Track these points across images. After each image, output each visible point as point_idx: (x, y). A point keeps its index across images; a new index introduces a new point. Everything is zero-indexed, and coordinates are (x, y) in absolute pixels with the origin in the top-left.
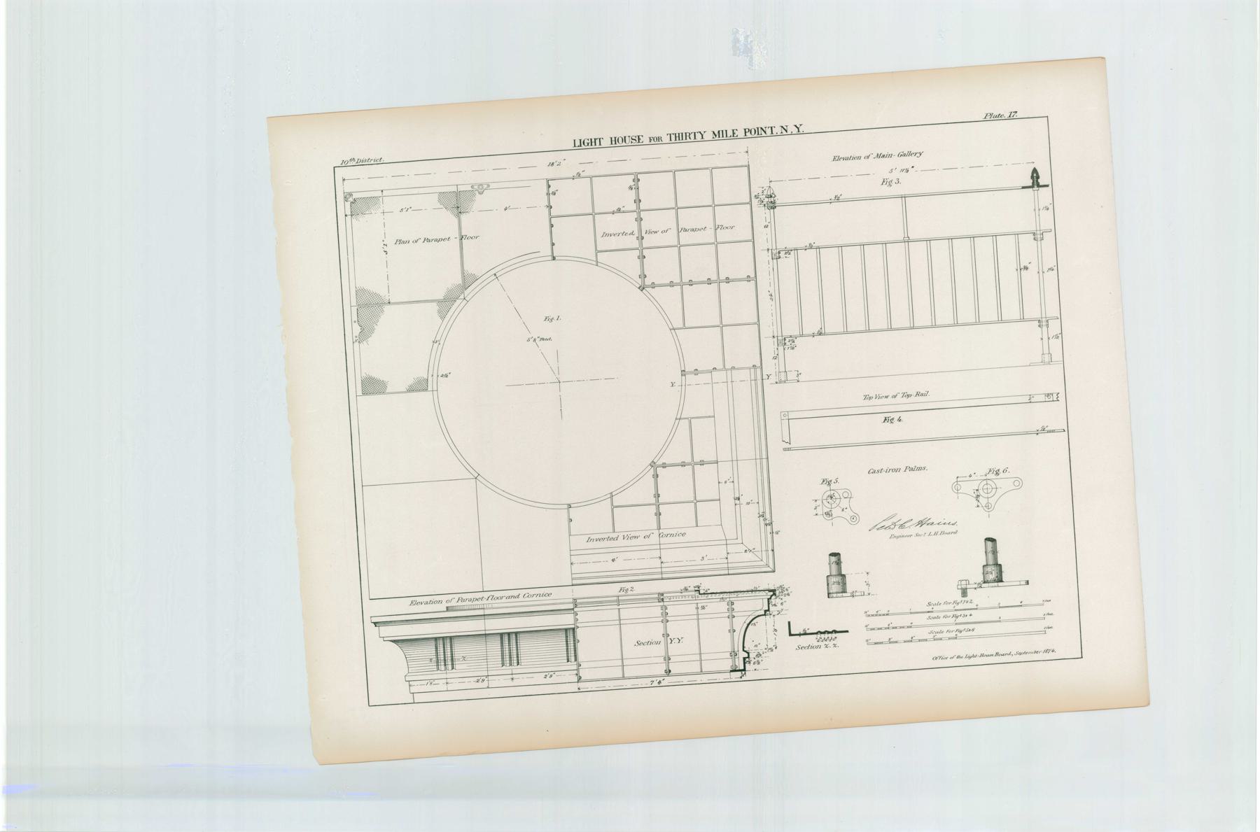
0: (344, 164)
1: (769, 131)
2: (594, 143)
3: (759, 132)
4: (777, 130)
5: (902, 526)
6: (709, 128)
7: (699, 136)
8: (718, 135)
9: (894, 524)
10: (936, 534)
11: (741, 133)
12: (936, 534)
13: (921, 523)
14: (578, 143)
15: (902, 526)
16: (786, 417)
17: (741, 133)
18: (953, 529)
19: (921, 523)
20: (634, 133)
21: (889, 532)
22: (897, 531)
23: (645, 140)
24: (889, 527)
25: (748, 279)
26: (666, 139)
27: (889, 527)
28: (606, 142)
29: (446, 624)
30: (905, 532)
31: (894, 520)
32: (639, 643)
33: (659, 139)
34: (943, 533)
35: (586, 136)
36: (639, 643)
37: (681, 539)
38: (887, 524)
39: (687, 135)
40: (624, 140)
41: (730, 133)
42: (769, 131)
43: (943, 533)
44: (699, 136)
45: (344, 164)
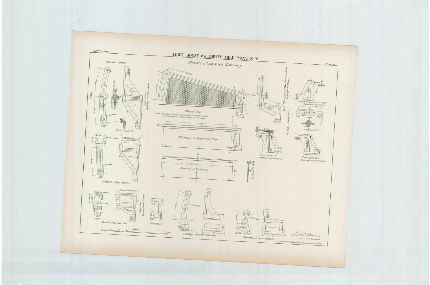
0: (94, 52)
2: (180, 55)
4: (231, 57)
5: (302, 235)
6: (224, 54)
7: (220, 57)
11: (235, 58)
13: (309, 235)
14: (175, 55)
15: (302, 235)
17: (235, 58)
18: (319, 238)
19: (309, 235)
20: (195, 53)
22: (300, 237)
24: (297, 235)
26: (207, 57)
27: (297, 235)
28: (185, 55)
30: (302, 237)
31: (300, 233)
33: (204, 56)
34: (315, 239)
35: (178, 52)
38: (297, 234)
40: (192, 55)
41: (231, 57)
42: (246, 59)
43: (315, 239)
44: (220, 57)
45: (94, 52)
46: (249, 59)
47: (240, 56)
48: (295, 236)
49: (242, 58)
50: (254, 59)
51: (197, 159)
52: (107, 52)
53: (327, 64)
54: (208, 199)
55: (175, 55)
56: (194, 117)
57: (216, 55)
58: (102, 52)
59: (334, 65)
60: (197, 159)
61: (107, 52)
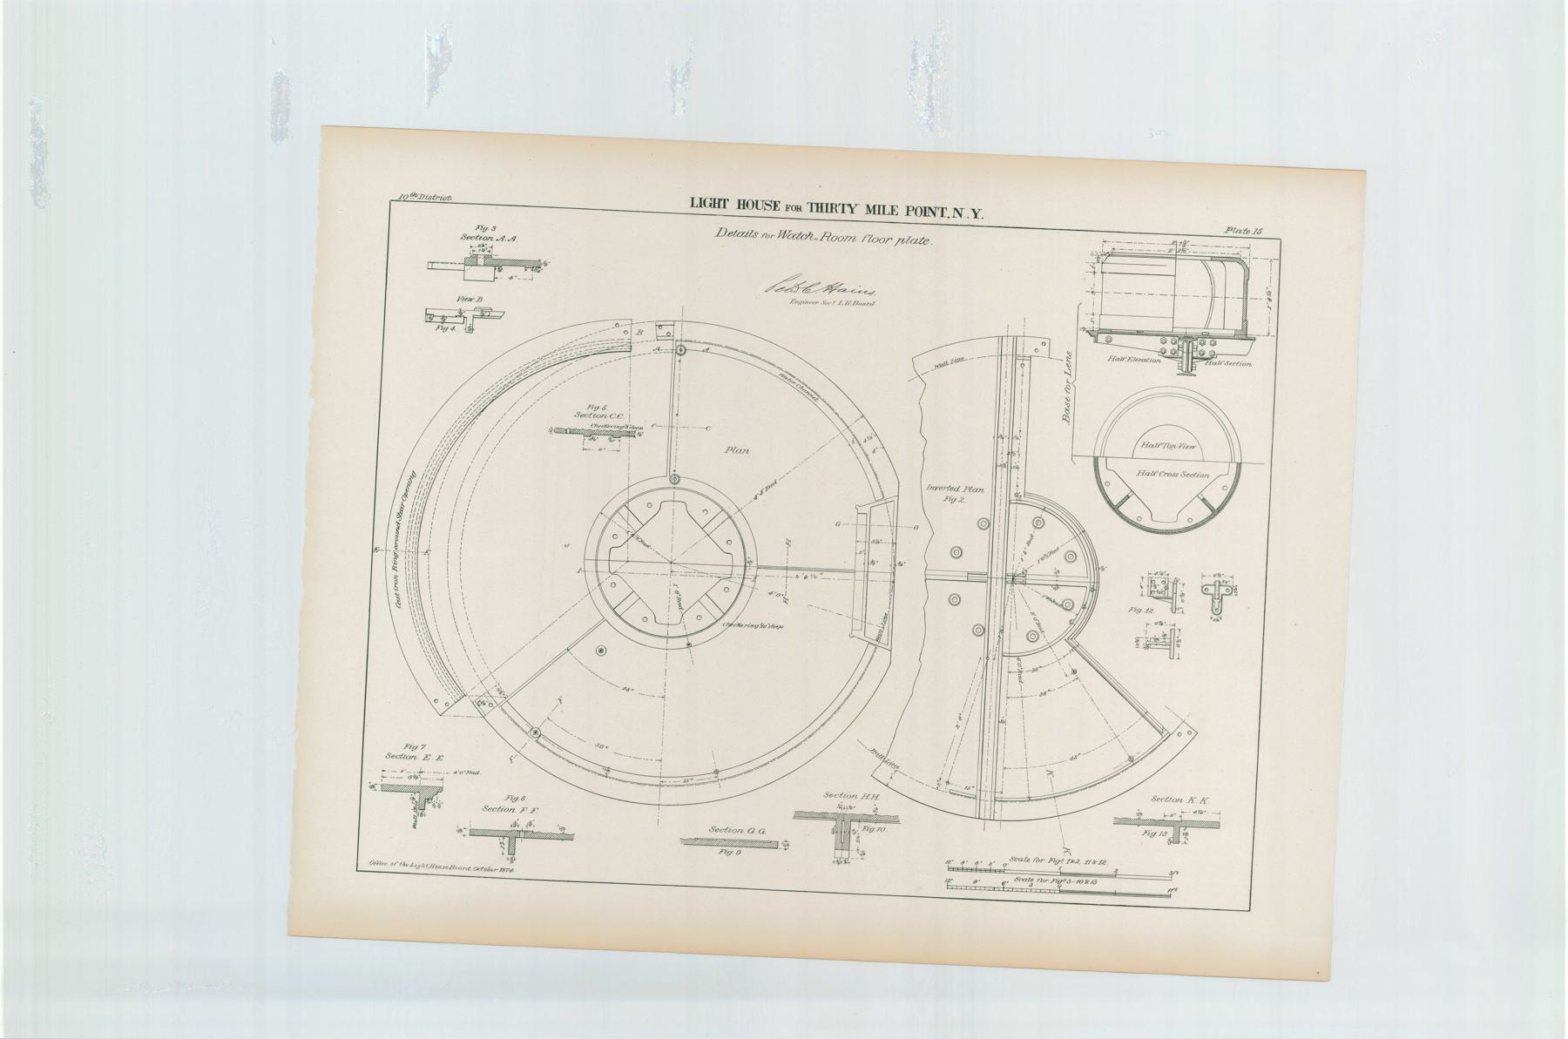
0: (403, 199)
4: (888, 210)
5: (806, 290)
6: (862, 199)
7: (847, 209)
9: (798, 286)
10: (848, 303)
11: (902, 210)
12: (848, 303)
13: (830, 288)
14: (697, 202)
15: (806, 290)
16: (942, 783)
17: (902, 210)
18: (870, 299)
19: (830, 288)
20: (768, 198)
21: (790, 296)
22: (800, 296)
24: (790, 290)
25: (1245, 327)
27: (790, 290)
30: (809, 297)
31: (798, 281)
32: (487, 808)
33: (798, 209)
34: (856, 303)
35: (708, 194)
36: (487, 808)
38: (788, 285)
39: (832, 208)
40: (755, 204)
41: (888, 210)
42: (939, 213)
43: (856, 303)
44: (847, 209)
45: (403, 199)
48: (782, 293)
49: (924, 211)
51: (717, 772)
52: (446, 200)
55: (697, 202)
56: (957, 741)
57: (717, 196)
58: (432, 199)
60: (717, 772)
61: (446, 200)
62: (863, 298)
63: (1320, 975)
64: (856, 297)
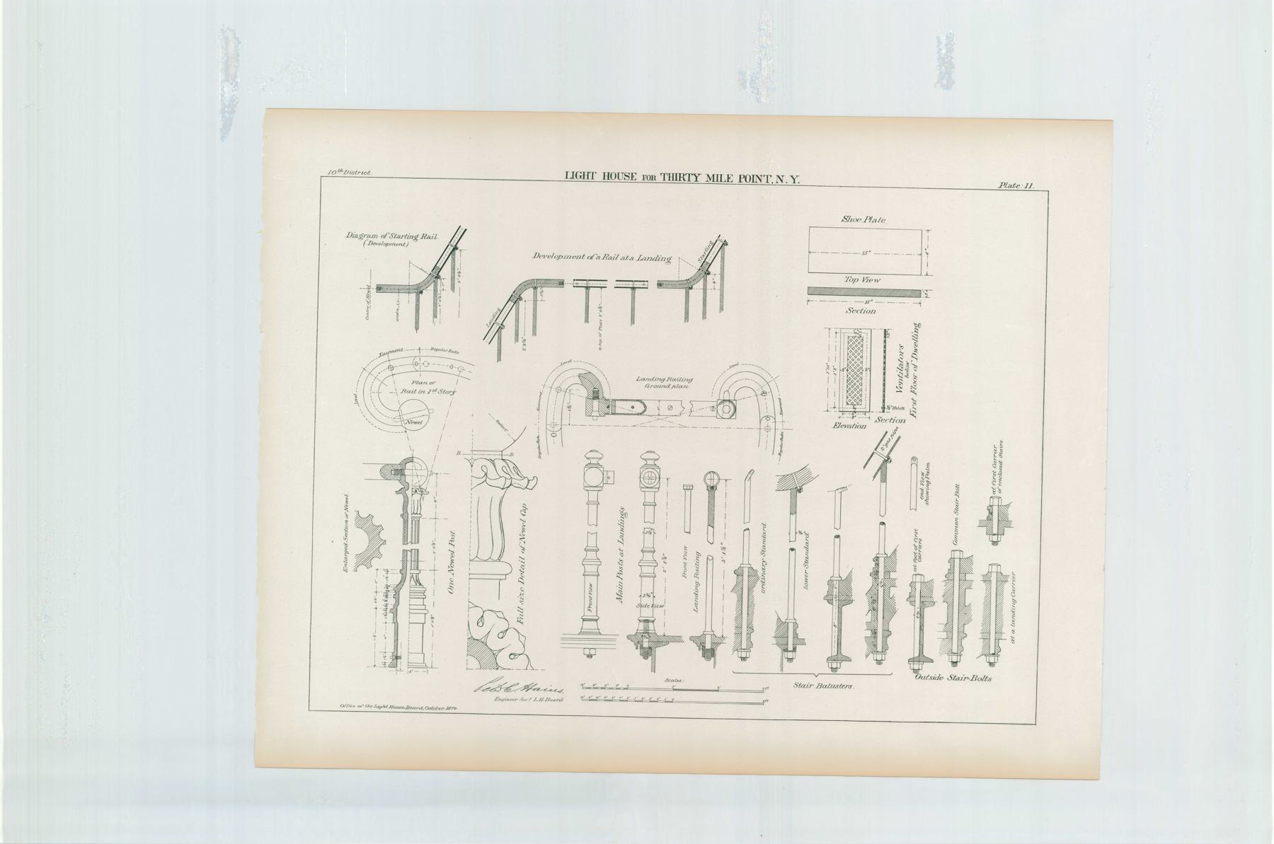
0: (332, 174)
1: (764, 180)
2: (586, 176)
3: (753, 179)
4: (725, 178)
5: (507, 689)
7: (693, 178)
8: (714, 179)
10: (541, 700)
11: (735, 179)
12: (541, 700)
13: (527, 688)
14: (570, 175)
15: (507, 689)
17: (735, 179)
19: (527, 688)
20: (629, 170)
21: (495, 694)
22: (502, 694)
23: (639, 178)
24: (494, 690)
27: (494, 690)
28: (599, 177)
29: (982, 607)
33: (653, 178)
34: (548, 699)
35: (580, 168)
37: (594, 588)
40: (617, 176)
41: (725, 178)
42: (764, 180)
43: (548, 699)
44: (693, 178)
45: (332, 174)
46: (774, 179)
47: (749, 172)
49: (752, 178)
50: (788, 180)
52: (366, 174)
53: (1004, 186)
54: (748, 483)
55: (570, 175)
57: (586, 171)
58: (353, 174)
59: (1029, 187)
61: (366, 174)
62: (621, 284)
63: (1092, 776)
64: (548, 694)
